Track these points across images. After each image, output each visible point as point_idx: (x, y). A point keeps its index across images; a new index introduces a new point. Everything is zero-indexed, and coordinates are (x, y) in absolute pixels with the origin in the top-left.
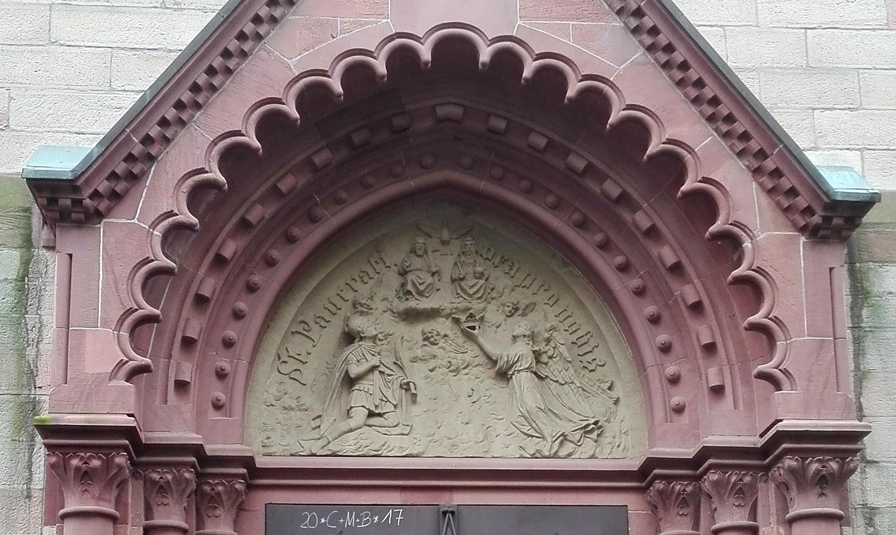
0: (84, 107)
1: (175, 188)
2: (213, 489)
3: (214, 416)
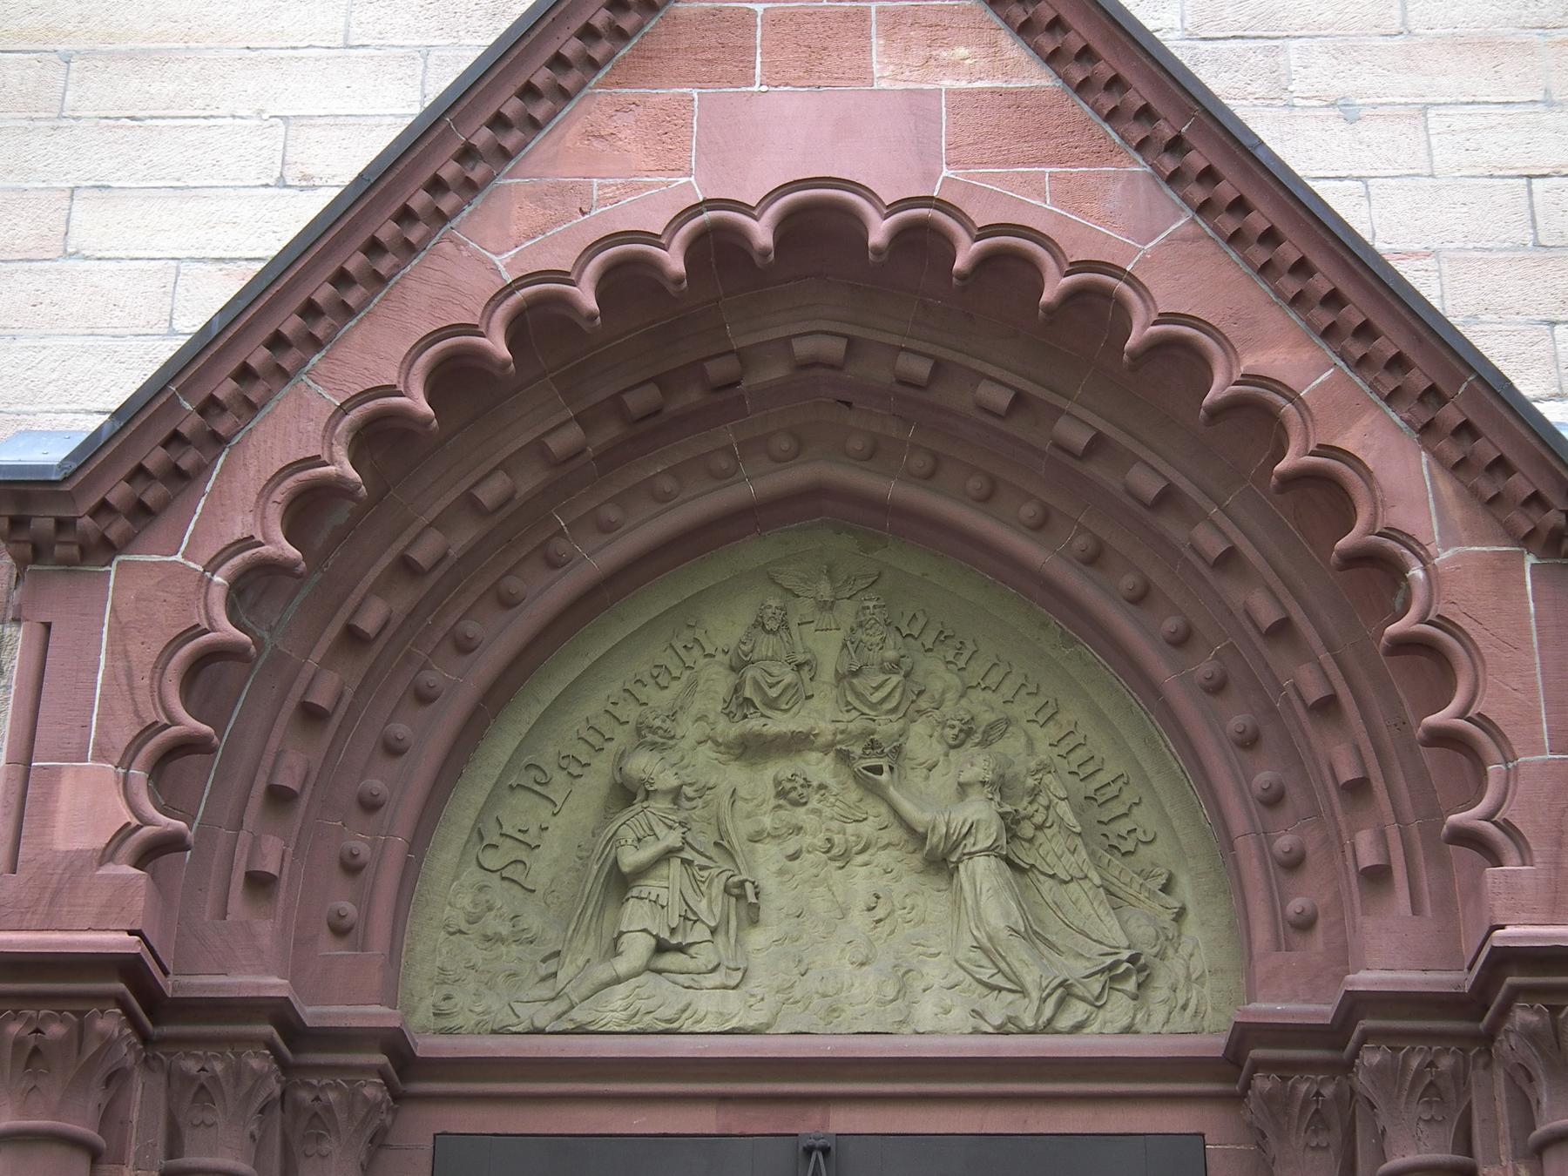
0: (118, 365)
1: (260, 495)
2: (317, 1099)
3: (329, 947)
